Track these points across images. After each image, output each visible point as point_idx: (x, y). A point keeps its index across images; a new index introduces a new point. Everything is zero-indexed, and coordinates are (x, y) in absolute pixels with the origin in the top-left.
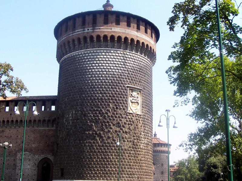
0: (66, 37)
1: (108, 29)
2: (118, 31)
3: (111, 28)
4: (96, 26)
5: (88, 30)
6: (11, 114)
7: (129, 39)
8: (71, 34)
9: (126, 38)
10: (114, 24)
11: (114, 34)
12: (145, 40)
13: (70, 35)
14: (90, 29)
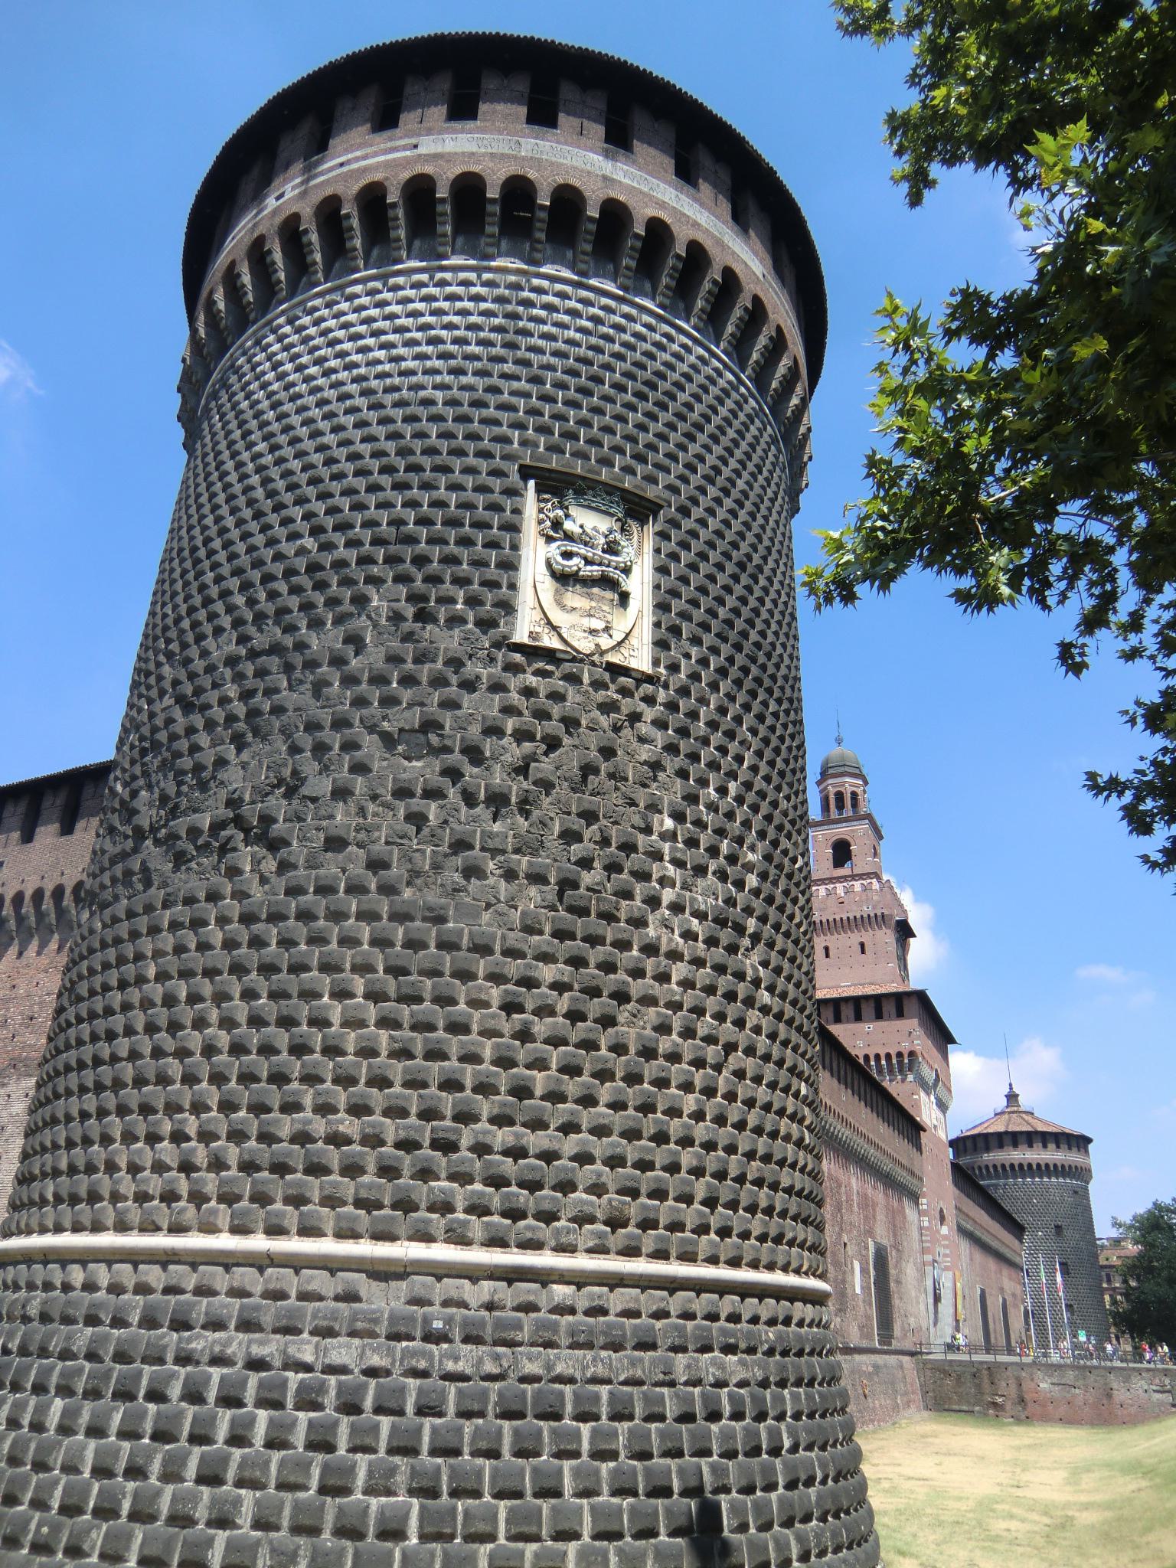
2: (458, 150)
3: (414, 141)
10: (440, 111)
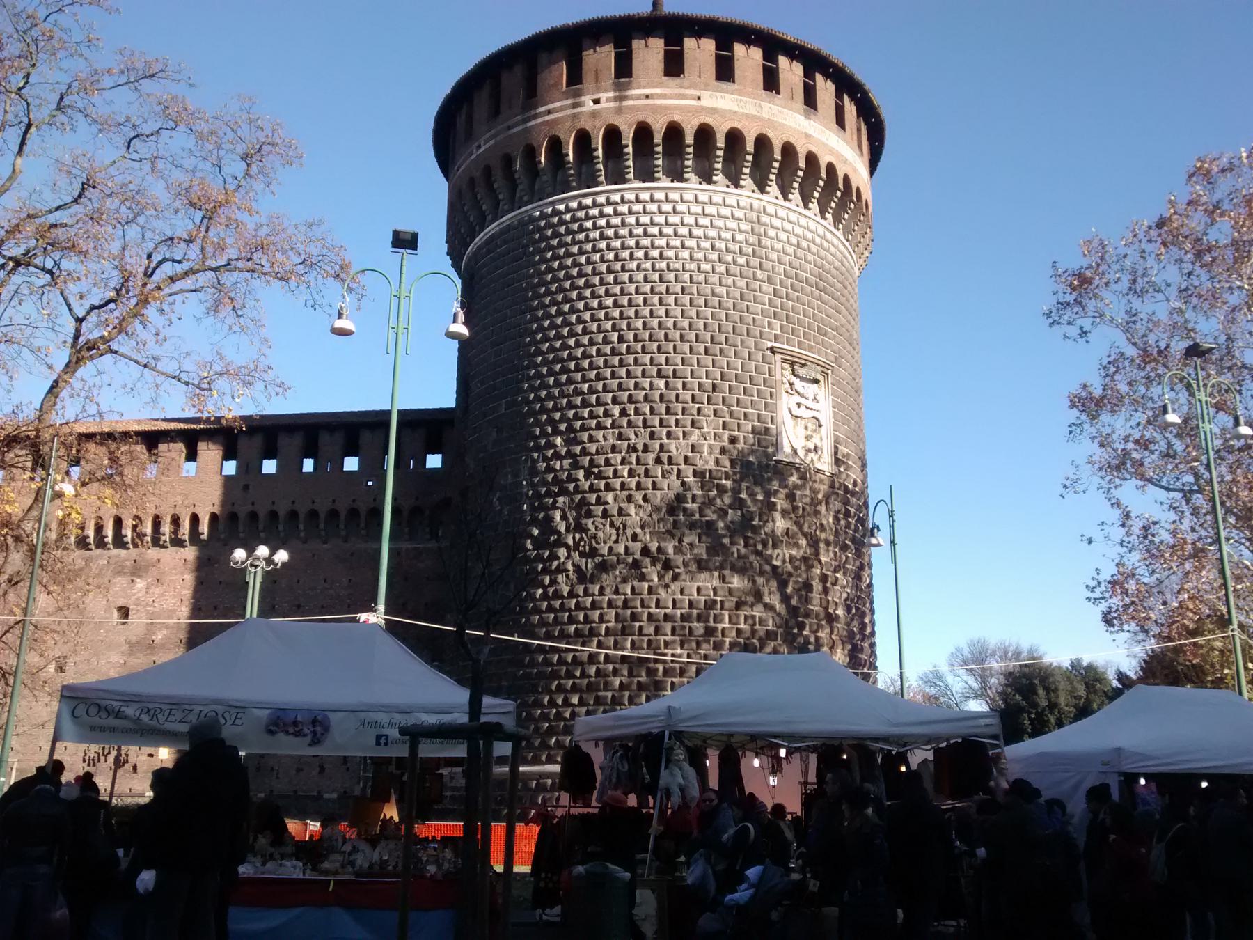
0: (492, 142)
1: (684, 97)
3: (697, 93)
4: (630, 83)
5: (596, 102)
6: (246, 487)
7: (719, 178)
8: (517, 124)
9: (762, 142)
11: (710, 120)
12: (839, 156)
13: (515, 130)
14: (603, 96)
